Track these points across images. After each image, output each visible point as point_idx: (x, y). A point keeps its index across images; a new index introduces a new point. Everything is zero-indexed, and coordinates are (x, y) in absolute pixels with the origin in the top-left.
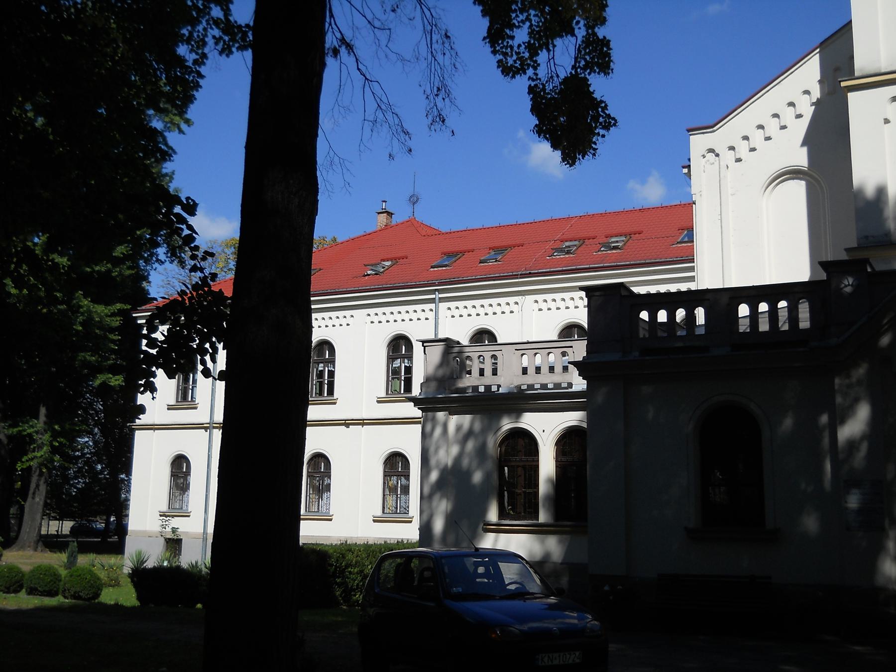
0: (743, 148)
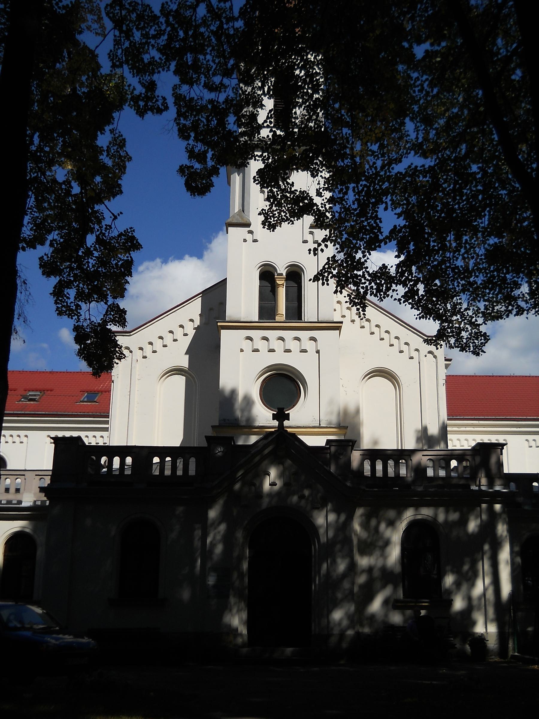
0: (148, 349)
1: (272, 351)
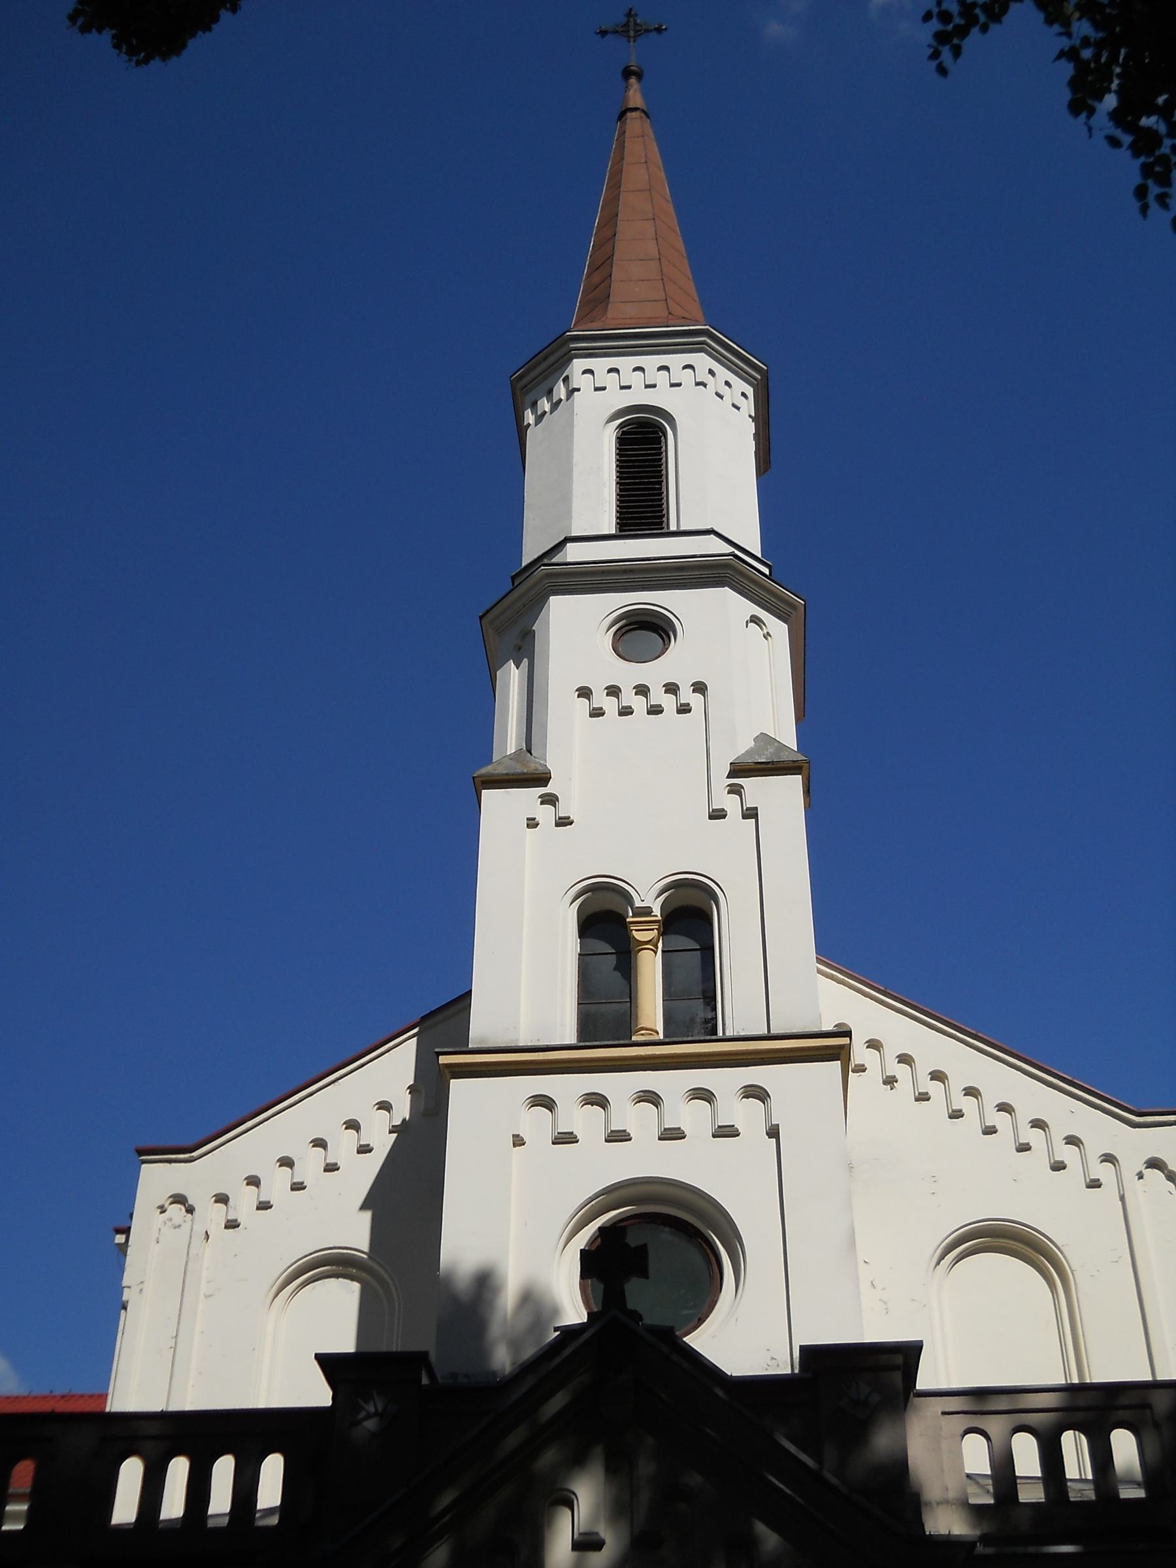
1: (618, 1137)
